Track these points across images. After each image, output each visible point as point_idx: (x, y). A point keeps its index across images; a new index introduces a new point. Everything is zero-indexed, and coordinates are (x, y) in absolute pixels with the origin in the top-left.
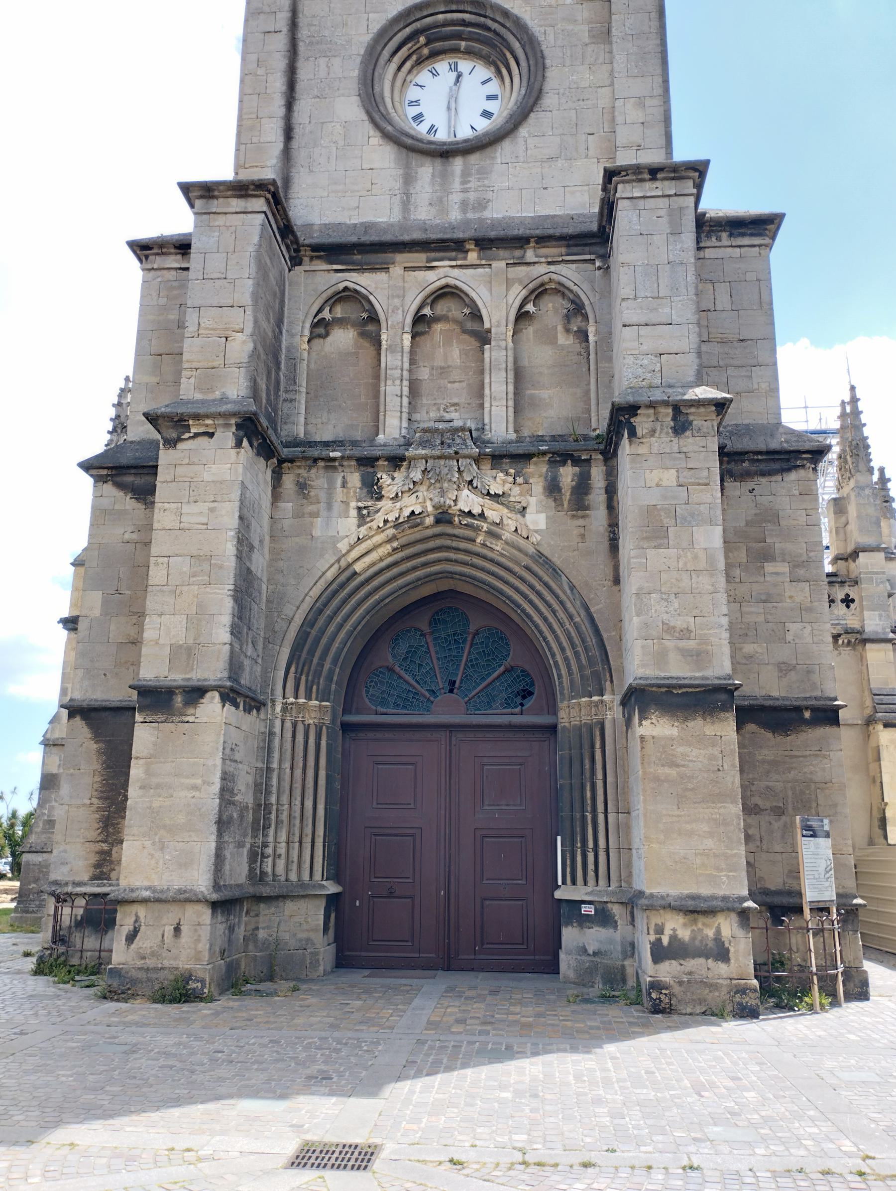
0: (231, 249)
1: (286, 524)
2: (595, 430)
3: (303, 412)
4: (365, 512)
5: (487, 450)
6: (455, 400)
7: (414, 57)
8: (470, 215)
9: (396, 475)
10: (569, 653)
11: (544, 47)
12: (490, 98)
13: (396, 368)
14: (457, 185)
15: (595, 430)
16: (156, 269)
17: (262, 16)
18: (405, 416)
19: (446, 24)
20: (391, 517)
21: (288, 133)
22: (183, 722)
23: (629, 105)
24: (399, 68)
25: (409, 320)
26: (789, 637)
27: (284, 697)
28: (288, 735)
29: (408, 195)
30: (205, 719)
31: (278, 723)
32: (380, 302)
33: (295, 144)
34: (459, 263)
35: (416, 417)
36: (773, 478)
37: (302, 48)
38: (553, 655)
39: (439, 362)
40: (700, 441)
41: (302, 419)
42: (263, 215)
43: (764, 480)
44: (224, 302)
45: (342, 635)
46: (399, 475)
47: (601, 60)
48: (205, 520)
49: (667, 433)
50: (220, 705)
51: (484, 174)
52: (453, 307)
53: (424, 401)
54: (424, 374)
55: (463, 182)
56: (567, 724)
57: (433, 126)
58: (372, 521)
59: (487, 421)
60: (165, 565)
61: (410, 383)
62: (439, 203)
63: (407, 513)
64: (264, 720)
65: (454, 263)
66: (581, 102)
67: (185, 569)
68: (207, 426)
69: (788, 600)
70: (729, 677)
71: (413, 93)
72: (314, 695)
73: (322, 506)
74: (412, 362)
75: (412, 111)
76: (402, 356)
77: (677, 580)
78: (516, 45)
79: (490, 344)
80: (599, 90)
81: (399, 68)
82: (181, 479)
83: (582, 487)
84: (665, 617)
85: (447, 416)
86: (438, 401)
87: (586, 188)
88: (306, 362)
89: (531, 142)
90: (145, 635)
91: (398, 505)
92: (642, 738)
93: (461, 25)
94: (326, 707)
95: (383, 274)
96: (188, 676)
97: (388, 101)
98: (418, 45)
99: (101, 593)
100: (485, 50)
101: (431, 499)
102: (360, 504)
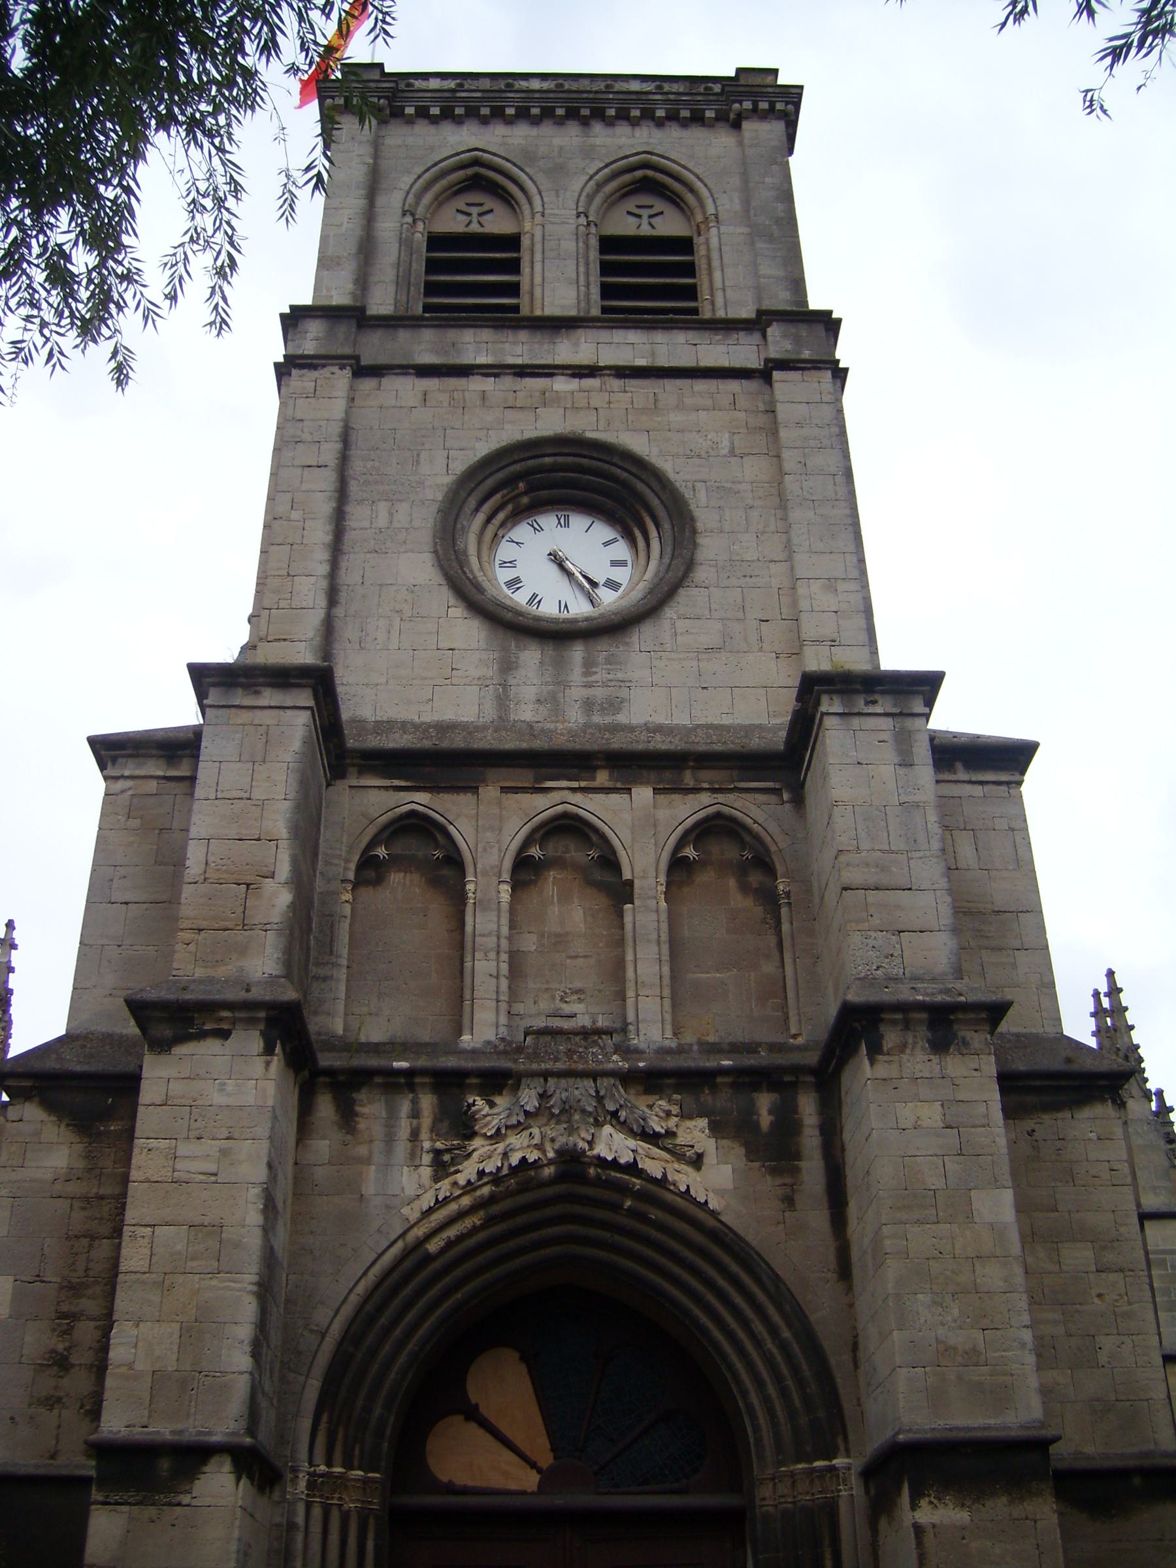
0: (259, 758)
1: (320, 1173)
2: (795, 1036)
3: (343, 995)
4: (447, 1157)
5: (641, 1064)
6: (578, 985)
7: (510, 507)
8: (597, 719)
9: (498, 1100)
10: (771, 1390)
11: (692, 507)
12: (615, 563)
13: (489, 935)
14: (576, 675)
15: (795, 1036)
16: (128, 777)
17: (301, 446)
18: (503, 1006)
19: (554, 468)
20: (490, 1167)
21: (333, 596)
22: (170, 1504)
23: (816, 587)
24: (489, 520)
25: (508, 864)
26: (1103, 1358)
27: (311, 1464)
28: (316, 1528)
29: (505, 686)
30: (207, 1501)
31: (301, 1508)
32: (463, 832)
33: (339, 611)
34: (583, 784)
35: (519, 1008)
36: (1060, 1115)
37: (354, 488)
38: (745, 1394)
39: (552, 926)
40: (973, 1061)
41: (341, 1007)
42: (309, 713)
43: (1047, 1118)
44: (245, 833)
45: (402, 1359)
46: (502, 1101)
47: (772, 528)
48: (212, 1168)
49: (923, 1049)
50: (231, 1478)
51: (616, 663)
52: (572, 847)
53: (531, 985)
54: (529, 943)
55: (587, 673)
56: (771, 1509)
57: (535, 596)
58: (457, 1172)
59: (631, 1017)
60: (147, 1240)
61: (510, 957)
62: (552, 702)
63: (515, 1160)
64: (278, 1503)
65: (575, 784)
66: (748, 579)
67: (179, 1247)
68: (221, 1019)
69: (1096, 1300)
70: (1043, 1425)
71: (505, 551)
72: (356, 1463)
73: (378, 1146)
74: (512, 926)
75: (504, 575)
76: (499, 917)
77: (953, 1272)
78: (655, 502)
79: (633, 903)
80: (772, 565)
81: (489, 520)
82: (177, 1102)
83: (787, 1124)
84: (941, 1331)
85: (567, 1009)
86: (553, 985)
87: (763, 691)
88: (348, 921)
89: (681, 625)
90: (112, 1354)
91: (501, 1147)
92: (918, 1529)
93: (579, 472)
94: (373, 1480)
95: (469, 795)
96: (180, 1427)
97: (474, 560)
98: (516, 492)
99: (11, 1279)
100: (609, 504)
101: (553, 1140)
102: (439, 1145)
